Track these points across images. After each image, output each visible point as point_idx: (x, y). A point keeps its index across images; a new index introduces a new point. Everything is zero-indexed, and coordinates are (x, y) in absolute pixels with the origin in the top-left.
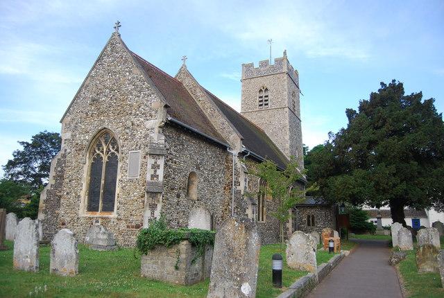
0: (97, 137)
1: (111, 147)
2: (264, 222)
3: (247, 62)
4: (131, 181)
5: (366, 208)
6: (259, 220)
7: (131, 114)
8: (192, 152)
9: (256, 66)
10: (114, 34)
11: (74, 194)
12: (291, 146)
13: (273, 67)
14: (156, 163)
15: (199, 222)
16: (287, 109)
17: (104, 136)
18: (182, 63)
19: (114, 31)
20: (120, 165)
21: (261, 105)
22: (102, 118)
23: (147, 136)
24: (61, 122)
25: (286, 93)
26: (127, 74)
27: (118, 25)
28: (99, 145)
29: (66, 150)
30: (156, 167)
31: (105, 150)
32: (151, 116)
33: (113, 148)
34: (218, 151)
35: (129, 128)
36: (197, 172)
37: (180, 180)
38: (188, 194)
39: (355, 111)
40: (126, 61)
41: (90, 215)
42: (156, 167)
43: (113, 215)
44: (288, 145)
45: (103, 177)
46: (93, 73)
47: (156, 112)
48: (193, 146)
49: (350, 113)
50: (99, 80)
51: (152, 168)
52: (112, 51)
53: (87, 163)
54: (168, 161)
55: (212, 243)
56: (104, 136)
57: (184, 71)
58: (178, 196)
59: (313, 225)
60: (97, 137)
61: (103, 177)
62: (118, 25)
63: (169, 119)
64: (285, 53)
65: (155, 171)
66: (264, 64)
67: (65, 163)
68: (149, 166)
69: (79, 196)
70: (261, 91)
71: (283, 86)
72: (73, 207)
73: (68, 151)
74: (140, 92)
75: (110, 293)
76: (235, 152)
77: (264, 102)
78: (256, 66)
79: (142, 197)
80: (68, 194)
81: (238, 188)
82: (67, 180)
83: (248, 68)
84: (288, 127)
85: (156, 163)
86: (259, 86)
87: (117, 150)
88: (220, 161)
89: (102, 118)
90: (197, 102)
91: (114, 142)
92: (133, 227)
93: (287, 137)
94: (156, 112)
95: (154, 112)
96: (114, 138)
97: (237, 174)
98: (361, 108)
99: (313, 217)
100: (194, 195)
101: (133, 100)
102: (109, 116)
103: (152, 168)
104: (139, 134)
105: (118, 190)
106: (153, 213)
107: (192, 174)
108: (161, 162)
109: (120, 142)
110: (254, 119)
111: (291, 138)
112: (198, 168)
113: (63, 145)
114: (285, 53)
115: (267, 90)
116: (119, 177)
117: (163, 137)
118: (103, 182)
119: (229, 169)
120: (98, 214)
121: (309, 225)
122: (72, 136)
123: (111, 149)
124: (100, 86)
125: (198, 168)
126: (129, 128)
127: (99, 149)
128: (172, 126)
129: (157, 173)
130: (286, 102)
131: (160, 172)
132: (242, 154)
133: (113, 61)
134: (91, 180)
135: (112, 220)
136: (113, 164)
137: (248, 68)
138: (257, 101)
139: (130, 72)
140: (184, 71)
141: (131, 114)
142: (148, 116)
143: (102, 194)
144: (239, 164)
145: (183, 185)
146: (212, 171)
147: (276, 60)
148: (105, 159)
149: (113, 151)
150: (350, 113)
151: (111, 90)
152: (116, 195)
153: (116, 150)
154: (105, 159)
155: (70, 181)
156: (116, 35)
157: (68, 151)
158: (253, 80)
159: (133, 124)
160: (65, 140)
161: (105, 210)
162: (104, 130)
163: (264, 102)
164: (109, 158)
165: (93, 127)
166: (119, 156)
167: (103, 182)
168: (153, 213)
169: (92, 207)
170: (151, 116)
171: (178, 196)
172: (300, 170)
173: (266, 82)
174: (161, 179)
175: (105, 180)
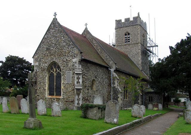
0: (51, 65)
1: (57, 69)
2: (127, 100)
3: (118, 19)
4: (68, 83)
5: (178, 92)
6: (124, 99)
7: (65, 56)
8: (93, 72)
9: (123, 21)
10: (54, 19)
11: (42, 88)
12: (142, 63)
13: (132, 21)
14: (78, 77)
15: (98, 101)
16: (140, 44)
17: (54, 65)
18: (85, 27)
19: (54, 17)
20: (62, 77)
21: (126, 40)
22: (52, 57)
23: (73, 65)
24: (33, 58)
25: (139, 36)
26: (62, 38)
27: (55, 14)
28: (52, 69)
29: (37, 70)
30: (78, 78)
31: (55, 71)
32: (75, 57)
33: (59, 70)
34: (105, 69)
35: (65, 62)
36: (96, 79)
37: (88, 83)
38: (92, 89)
39: (173, 47)
40: (61, 32)
41: (50, 97)
42: (78, 78)
43: (61, 97)
44: (140, 63)
45: (55, 82)
46: (46, 36)
47: (77, 55)
48: (93, 68)
49: (171, 48)
50: (49, 40)
51: (77, 79)
52: (54, 27)
53: (47, 76)
54: (83, 75)
55: (105, 109)
56: (54, 65)
57: (86, 31)
58: (88, 90)
59: (152, 101)
60: (51, 65)
61: (55, 82)
62: (55, 14)
63: (83, 58)
64: (139, 14)
65: (78, 80)
66: (127, 20)
67: (37, 75)
68: (76, 78)
69: (45, 89)
70: (126, 35)
71: (137, 32)
72: (43, 93)
73: (38, 70)
74: (69, 46)
75: (22, 134)
76: (112, 70)
77: (127, 40)
78: (123, 21)
79: (73, 90)
80: (40, 88)
81: (115, 85)
82: (39, 83)
83: (118, 22)
84: (140, 53)
85: (78, 77)
86: (125, 32)
87: (60, 71)
88: (105, 74)
89: (52, 57)
90: (94, 46)
91: (59, 67)
92: (70, 102)
93: (140, 59)
94: (77, 55)
95: (76, 55)
96: (58, 66)
97: (114, 80)
98: (152, 75)
99: (152, 97)
100: (95, 90)
101: (66, 50)
102: (55, 56)
103: (77, 79)
104: (70, 64)
105: (62, 87)
106: (78, 97)
107: (94, 80)
108: (81, 77)
109: (62, 67)
110: (122, 50)
111: (142, 59)
112: (96, 78)
113: (35, 68)
114: (139, 14)
115: (129, 34)
116: (62, 82)
117: (81, 66)
118: (55, 84)
119: (110, 77)
120: (54, 97)
121: (150, 101)
122: (39, 64)
123: (57, 70)
124: (50, 43)
125: (96, 78)
126: (65, 62)
127: (52, 70)
128: (84, 62)
129: (79, 81)
130: (139, 40)
131: (81, 81)
132: (117, 71)
133: (55, 31)
134: (49, 83)
135: (61, 99)
136: (59, 76)
137: (118, 22)
138: (124, 40)
139: (63, 37)
140: (86, 31)
141: (65, 56)
142: (74, 56)
143: (55, 89)
144: (115, 74)
145: (90, 85)
146: (102, 78)
147: (134, 18)
148: (55, 74)
149: (58, 71)
150: (171, 48)
151: (55, 45)
152: (62, 89)
153: (60, 71)
154: (55, 74)
155: (40, 83)
156: (55, 19)
157: (38, 70)
158: (121, 29)
159: (67, 60)
160: (36, 66)
161: (57, 95)
162: (54, 62)
163: (127, 40)
164: (57, 74)
165: (49, 60)
166: (62, 73)
167: (55, 84)
168: (78, 97)
169: (51, 94)
170: (75, 57)
171: (88, 90)
172: (147, 76)
173: (129, 30)
174: (81, 83)
175: (56, 83)
